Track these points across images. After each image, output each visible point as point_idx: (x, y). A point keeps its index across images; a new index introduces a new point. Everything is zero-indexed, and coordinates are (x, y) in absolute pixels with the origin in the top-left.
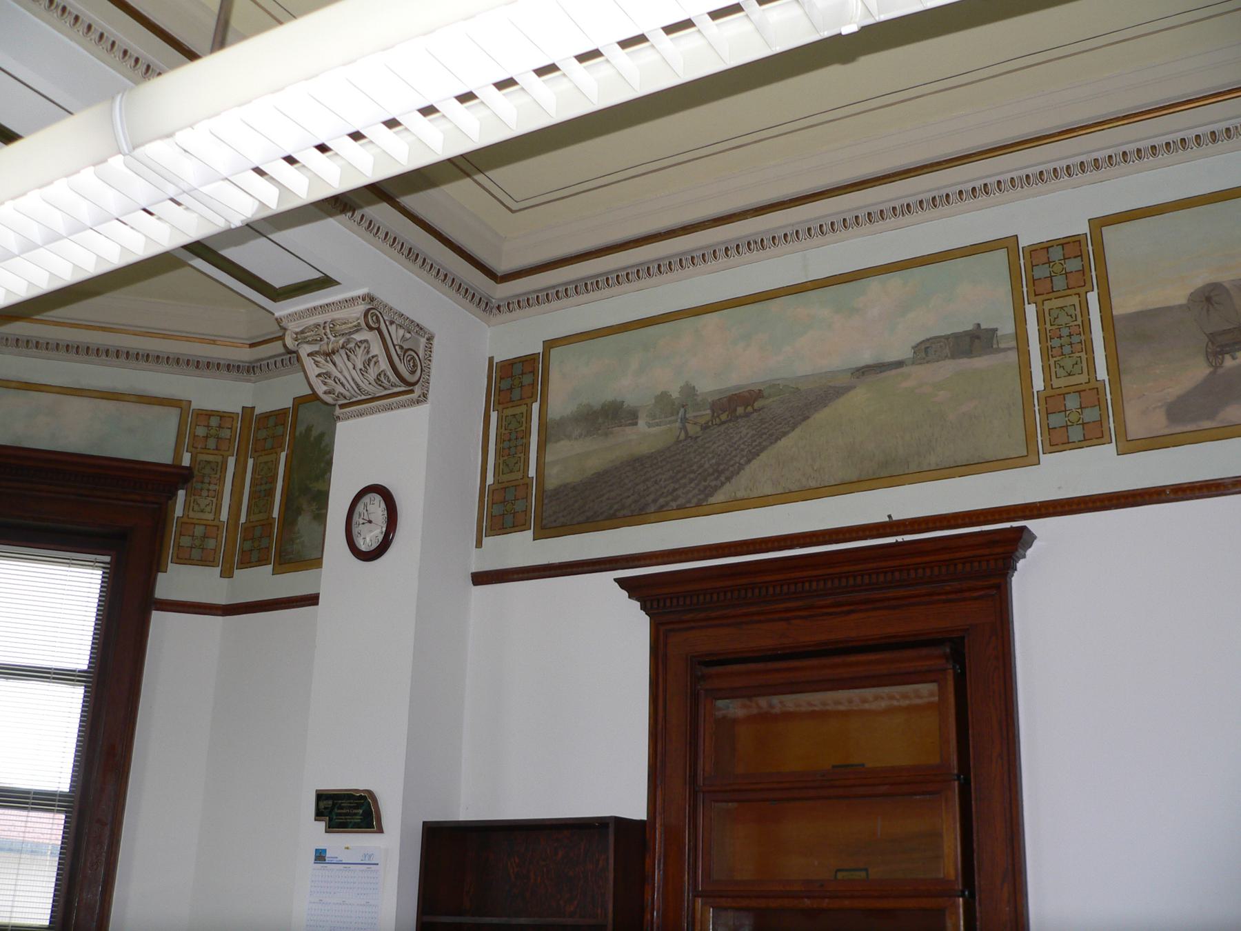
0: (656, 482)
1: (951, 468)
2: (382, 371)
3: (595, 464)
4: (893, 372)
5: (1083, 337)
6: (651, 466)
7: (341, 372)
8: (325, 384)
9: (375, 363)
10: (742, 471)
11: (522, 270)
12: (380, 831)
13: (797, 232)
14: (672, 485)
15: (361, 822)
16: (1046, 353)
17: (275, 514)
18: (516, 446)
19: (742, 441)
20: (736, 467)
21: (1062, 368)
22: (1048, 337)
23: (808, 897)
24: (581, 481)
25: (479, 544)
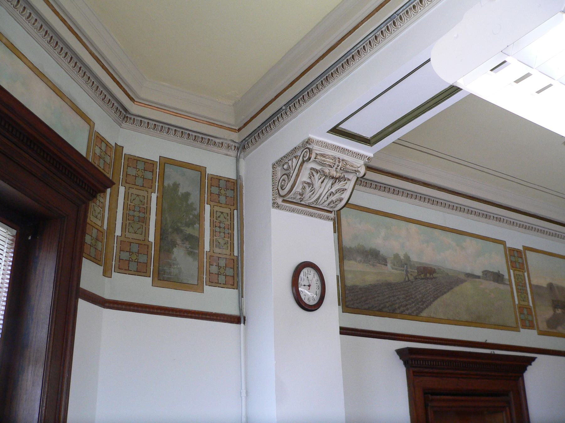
5: (230, 231)
14: (405, 302)
17: (152, 238)
22: (128, 208)
24: (364, 286)
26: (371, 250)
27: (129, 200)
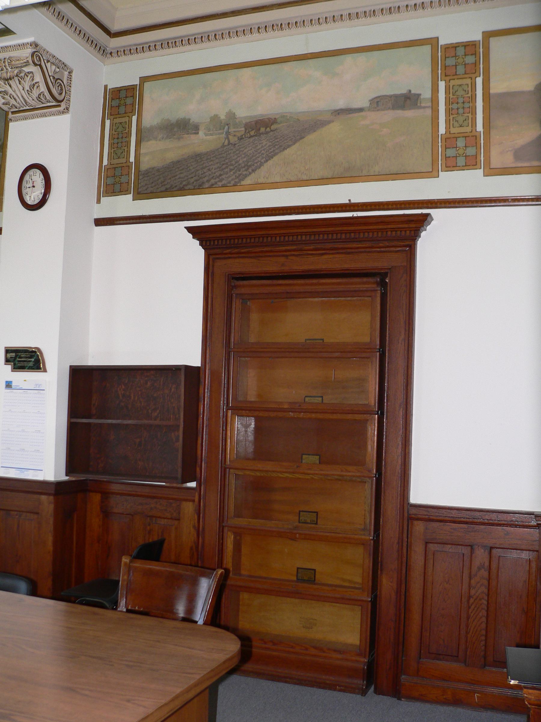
0: (209, 170)
1: (387, 175)
2: (41, 92)
3: (172, 156)
4: (357, 115)
5: (471, 104)
6: (206, 160)
7: (14, 91)
8: (4, 98)
9: (37, 87)
10: (262, 166)
11: (128, 31)
12: (45, 371)
13: (304, 21)
14: (220, 172)
15: (34, 366)
16: (449, 112)
18: (122, 142)
19: (263, 148)
20: (259, 164)
21: (457, 122)
23: (291, 412)
24: (163, 166)
25: (99, 201)
26: (177, 121)
27: (114, 130)
